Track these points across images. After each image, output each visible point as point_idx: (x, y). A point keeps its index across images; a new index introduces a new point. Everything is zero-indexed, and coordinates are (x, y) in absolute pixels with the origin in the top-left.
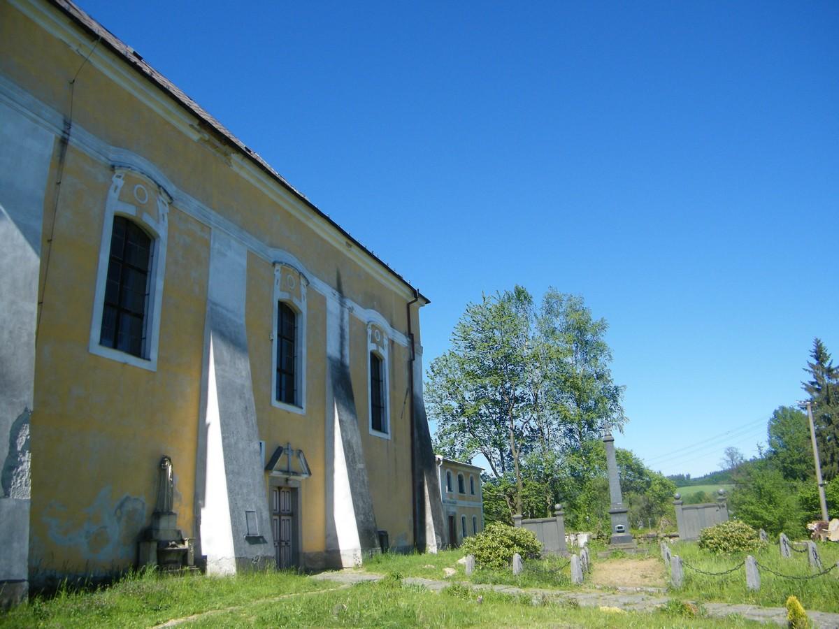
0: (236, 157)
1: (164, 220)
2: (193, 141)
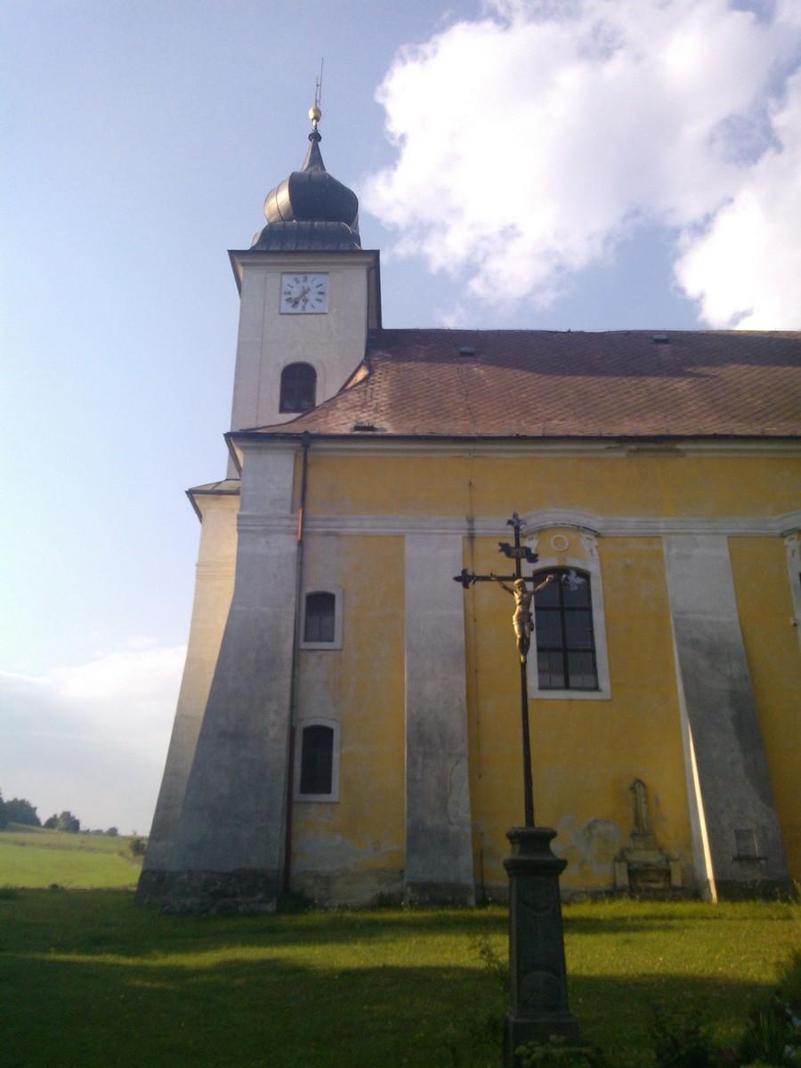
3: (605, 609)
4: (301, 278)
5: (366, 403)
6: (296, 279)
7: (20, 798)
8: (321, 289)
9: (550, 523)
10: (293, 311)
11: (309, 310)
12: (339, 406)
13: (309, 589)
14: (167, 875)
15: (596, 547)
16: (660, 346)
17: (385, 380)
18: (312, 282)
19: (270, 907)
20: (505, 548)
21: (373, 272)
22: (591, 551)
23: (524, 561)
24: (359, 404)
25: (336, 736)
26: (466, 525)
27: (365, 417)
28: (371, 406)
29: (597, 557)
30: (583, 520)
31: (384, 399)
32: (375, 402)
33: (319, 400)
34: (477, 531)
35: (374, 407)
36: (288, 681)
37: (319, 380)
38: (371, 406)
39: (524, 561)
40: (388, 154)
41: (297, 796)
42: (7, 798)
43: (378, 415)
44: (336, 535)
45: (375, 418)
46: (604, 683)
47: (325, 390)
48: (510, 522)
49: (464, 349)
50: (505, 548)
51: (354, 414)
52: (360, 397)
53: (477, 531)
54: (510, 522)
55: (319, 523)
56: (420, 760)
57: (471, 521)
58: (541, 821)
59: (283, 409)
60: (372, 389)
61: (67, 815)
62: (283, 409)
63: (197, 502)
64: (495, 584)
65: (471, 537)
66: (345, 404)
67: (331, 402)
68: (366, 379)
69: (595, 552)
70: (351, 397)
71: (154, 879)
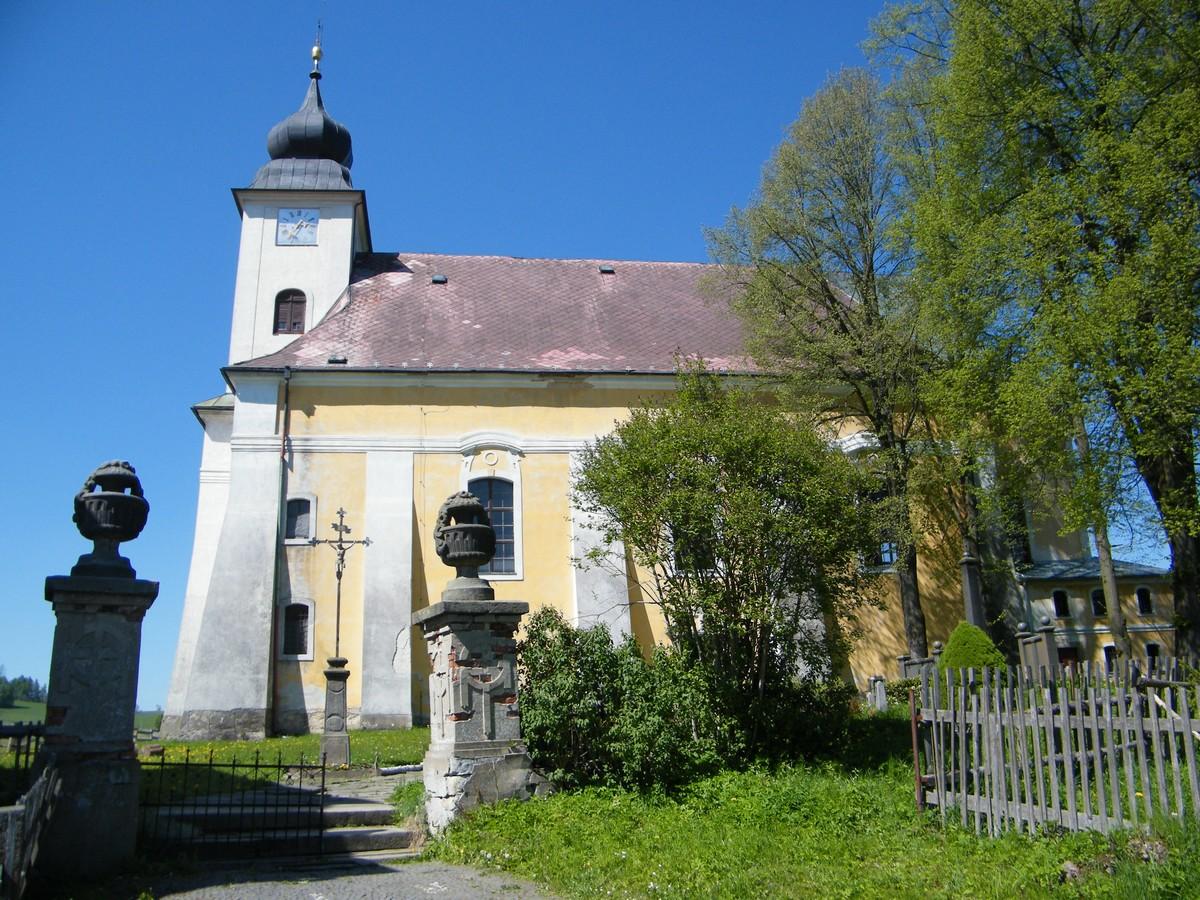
0: (590, 381)
2: (544, 389)
4: (295, 212)
5: (343, 333)
7: (26, 676)
12: (320, 336)
13: (289, 497)
16: (605, 276)
19: (261, 734)
20: (335, 526)
21: (360, 207)
23: (344, 533)
24: (337, 334)
25: (311, 610)
27: (339, 349)
28: (347, 336)
29: (518, 468)
31: (359, 329)
32: (351, 331)
33: (307, 328)
37: (308, 304)
38: (347, 336)
39: (344, 533)
40: (214, 439)
41: (282, 656)
42: (11, 676)
43: (351, 346)
45: (349, 349)
46: (518, 567)
47: (313, 316)
48: (338, 513)
49: (437, 277)
50: (335, 526)
51: (332, 344)
54: (338, 513)
58: (342, 656)
62: (276, 331)
63: (201, 416)
68: (347, 306)
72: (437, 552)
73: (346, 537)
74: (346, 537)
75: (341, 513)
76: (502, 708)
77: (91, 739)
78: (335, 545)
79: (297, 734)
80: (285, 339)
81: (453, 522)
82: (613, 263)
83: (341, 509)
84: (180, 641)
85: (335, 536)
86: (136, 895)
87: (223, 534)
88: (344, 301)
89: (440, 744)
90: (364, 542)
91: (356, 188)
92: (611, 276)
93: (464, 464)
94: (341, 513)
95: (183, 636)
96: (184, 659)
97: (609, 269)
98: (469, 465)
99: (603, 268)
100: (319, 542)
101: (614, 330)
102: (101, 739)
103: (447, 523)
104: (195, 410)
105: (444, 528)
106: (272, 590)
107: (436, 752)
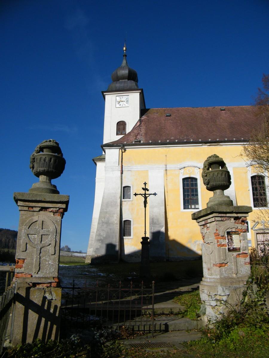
1: (198, 174)
3: (201, 188)
6: (120, 98)
8: (127, 100)
9: (187, 166)
10: (119, 106)
11: (124, 106)
12: (131, 134)
13: (123, 186)
14: (96, 315)
15: (199, 171)
16: (223, 111)
17: (145, 125)
18: (124, 98)
20: (143, 189)
22: (197, 173)
23: (146, 191)
26: (165, 167)
30: (195, 165)
32: (142, 132)
34: (167, 168)
35: (141, 134)
36: (119, 209)
39: (146, 191)
43: (142, 137)
44: (130, 171)
45: (141, 138)
47: (129, 129)
49: (167, 115)
50: (143, 189)
52: (137, 131)
53: (167, 168)
55: (126, 168)
56: (153, 228)
57: (166, 166)
59: (117, 134)
60: (141, 128)
61: (67, 247)
62: (117, 134)
64: (141, 195)
65: (166, 170)
66: (133, 133)
67: (130, 133)
68: (140, 125)
69: (199, 173)
70: (135, 131)
71: (90, 257)
72: (204, 183)
73: (147, 193)
74: (147, 193)
75: (145, 184)
76: (242, 260)
77: (37, 276)
78: (143, 195)
79: (129, 199)
80: (120, 137)
81: (210, 169)
82: (224, 107)
83: (145, 182)
84: (91, 232)
85: (143, 192)
86: (64, 357)
87: (103, 198)
88: (138, 124)
89: (210, 278)
90: (154, 194)
91: (139, 88)
92: (224, 111)
93: (181, 173)
94: (145, 184)
95: (92, 230)
96: (92, 238)
97: (224, 109)
98: (182, 173)
99: (221, 109)
100: (137, 194)
101: (228, 126)
102: (41, 276)
103: (208, 169)
104: (93, 160)
105: (207, 171)
106: (119, 216)
107: (207, 282)
